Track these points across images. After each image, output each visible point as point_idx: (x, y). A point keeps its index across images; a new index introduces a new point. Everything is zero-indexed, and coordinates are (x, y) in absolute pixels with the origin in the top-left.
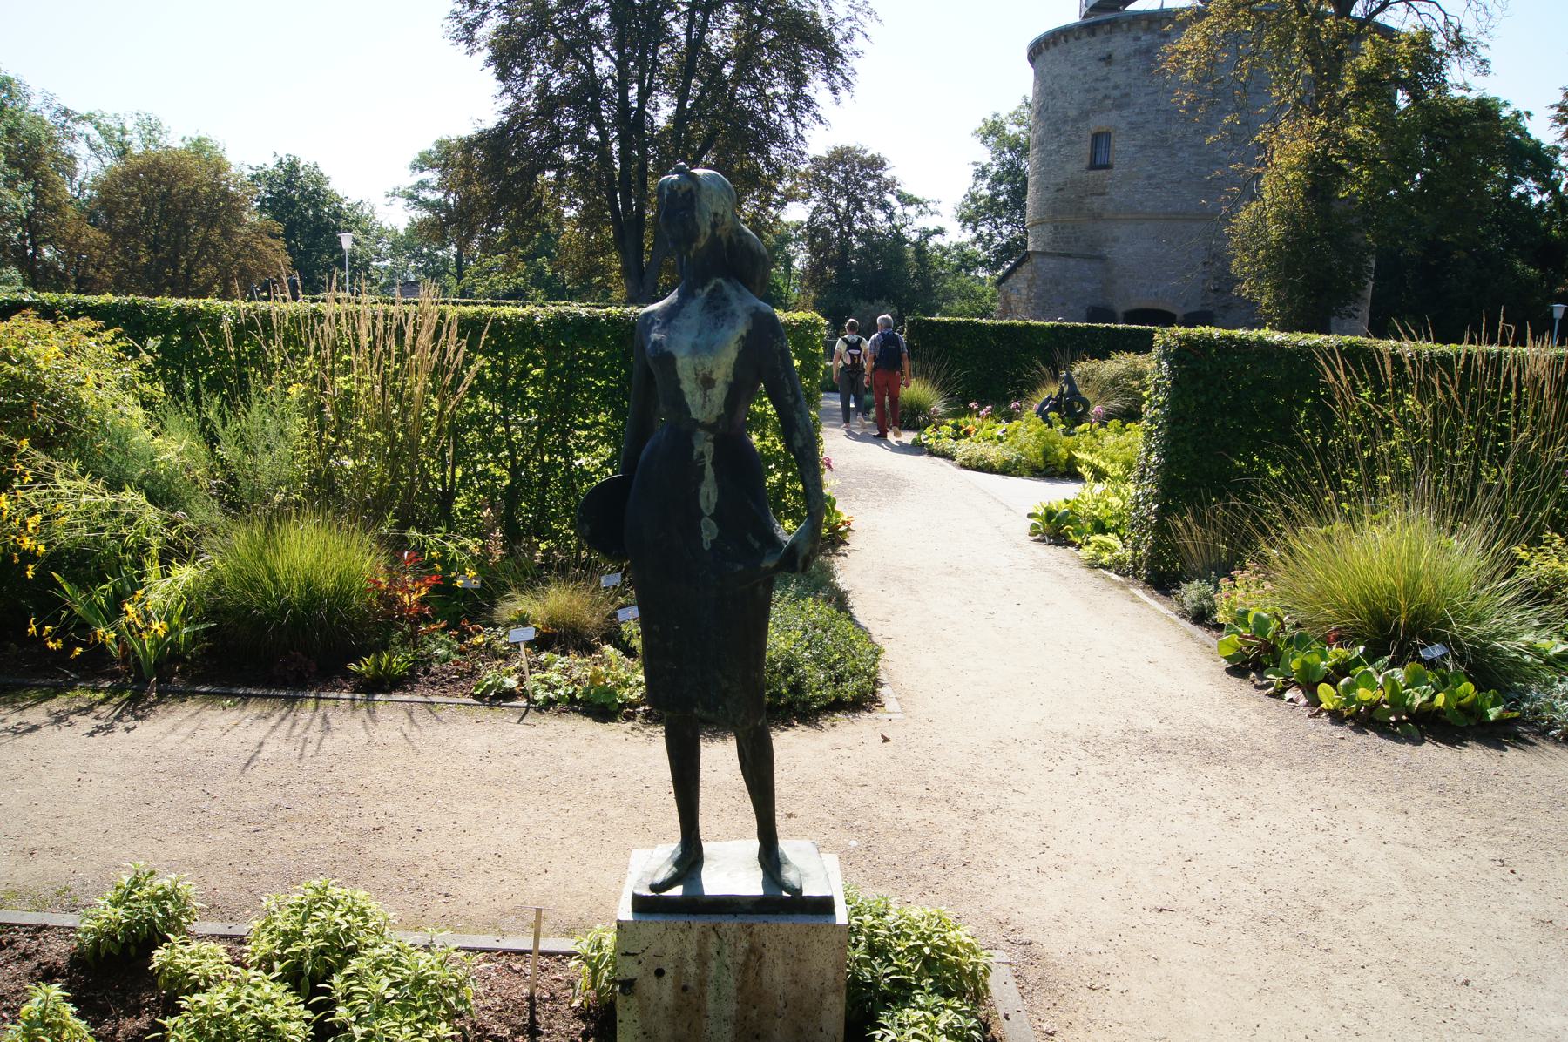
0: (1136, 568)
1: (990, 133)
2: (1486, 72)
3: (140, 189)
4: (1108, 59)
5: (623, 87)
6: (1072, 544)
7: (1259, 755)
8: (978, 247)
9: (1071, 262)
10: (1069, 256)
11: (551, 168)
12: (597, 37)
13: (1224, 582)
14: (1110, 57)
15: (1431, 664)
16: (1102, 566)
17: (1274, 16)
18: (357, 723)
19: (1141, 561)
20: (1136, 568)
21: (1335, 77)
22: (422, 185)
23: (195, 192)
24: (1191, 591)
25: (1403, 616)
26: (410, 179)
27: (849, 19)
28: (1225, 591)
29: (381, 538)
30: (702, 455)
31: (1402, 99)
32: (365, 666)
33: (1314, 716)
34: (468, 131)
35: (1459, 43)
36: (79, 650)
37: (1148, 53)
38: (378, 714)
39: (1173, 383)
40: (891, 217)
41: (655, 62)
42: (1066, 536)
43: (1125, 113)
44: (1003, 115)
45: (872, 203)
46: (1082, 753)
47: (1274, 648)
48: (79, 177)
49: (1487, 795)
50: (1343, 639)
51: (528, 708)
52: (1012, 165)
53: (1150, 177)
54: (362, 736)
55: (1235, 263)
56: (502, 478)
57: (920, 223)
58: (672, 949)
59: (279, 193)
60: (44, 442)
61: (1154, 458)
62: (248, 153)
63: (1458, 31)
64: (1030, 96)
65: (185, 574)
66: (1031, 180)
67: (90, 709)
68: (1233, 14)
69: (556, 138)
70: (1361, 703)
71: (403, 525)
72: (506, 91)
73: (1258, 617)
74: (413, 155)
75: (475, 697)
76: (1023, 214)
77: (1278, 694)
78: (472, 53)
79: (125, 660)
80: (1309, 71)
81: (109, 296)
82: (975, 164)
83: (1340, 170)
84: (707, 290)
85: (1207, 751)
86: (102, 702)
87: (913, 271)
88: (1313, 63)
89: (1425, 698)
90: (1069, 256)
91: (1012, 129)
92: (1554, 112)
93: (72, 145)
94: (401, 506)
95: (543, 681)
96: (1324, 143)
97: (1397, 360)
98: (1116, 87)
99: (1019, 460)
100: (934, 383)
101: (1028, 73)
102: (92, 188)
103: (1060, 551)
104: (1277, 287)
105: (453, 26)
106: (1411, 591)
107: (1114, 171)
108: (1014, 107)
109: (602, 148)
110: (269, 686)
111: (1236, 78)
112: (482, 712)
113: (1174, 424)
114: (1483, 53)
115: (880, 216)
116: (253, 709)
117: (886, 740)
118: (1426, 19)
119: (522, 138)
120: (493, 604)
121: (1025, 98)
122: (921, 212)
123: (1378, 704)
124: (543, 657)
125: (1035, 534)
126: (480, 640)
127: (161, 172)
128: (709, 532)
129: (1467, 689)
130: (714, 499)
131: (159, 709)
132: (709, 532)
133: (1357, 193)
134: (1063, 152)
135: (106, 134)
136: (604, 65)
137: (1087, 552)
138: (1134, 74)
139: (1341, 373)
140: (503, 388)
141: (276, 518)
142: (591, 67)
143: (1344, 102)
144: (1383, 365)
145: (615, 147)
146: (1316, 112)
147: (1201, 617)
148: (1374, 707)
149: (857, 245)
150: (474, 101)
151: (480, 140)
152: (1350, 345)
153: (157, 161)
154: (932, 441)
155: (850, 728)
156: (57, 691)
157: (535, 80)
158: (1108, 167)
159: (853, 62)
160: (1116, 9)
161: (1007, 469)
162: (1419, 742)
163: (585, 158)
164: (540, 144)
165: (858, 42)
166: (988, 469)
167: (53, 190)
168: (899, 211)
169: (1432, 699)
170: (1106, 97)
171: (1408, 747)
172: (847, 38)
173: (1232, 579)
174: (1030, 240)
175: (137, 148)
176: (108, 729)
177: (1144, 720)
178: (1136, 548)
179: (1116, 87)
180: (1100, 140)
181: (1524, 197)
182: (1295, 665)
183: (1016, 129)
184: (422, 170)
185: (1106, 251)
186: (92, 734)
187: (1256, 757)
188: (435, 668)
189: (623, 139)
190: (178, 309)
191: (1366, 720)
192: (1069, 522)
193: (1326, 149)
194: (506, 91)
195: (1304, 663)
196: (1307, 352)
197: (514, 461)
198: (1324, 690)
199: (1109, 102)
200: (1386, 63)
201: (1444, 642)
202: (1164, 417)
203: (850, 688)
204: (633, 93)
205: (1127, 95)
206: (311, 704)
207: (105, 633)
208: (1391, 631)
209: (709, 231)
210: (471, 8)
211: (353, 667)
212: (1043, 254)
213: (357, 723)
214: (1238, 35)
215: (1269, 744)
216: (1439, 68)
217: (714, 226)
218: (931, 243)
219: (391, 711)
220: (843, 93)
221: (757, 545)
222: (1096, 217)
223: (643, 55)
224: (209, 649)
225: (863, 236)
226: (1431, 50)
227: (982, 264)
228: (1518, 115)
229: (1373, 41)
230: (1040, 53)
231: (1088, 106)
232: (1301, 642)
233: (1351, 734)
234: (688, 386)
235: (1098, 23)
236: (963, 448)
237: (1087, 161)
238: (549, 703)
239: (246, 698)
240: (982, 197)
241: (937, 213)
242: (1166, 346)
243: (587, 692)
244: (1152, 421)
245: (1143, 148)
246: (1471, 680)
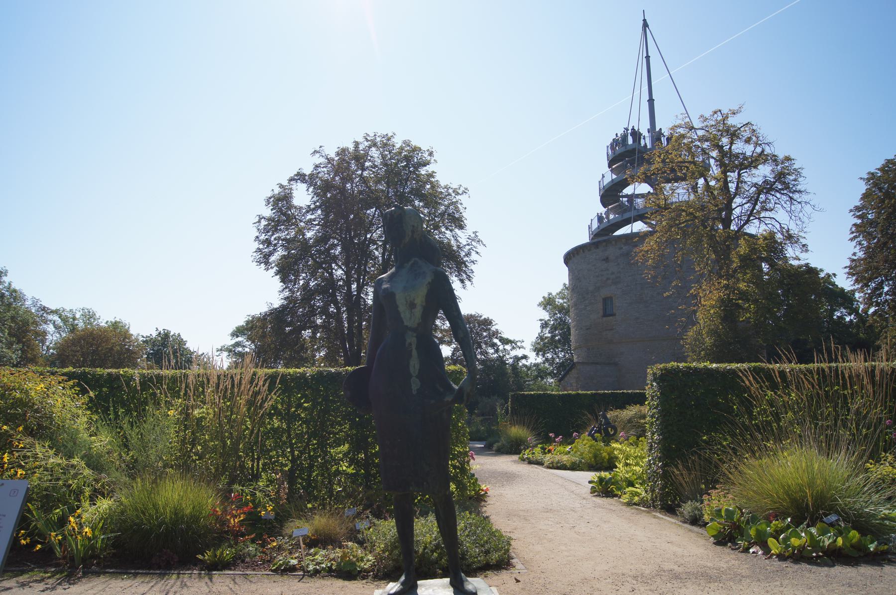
0: (654, 502)
1: (548, 304)
2: (807, 251)
3: (82, 348)
4: (606, 260)
5: (348, 283)
6: (616, 496)
7: (739, 577)
8: (547, 365)
10: (597, 363)
11: (309, 328)
12: (334, 259)
13: (705, 497)
15: (832, 525)
16: (635, 504)
17: (690, 230)
18: (203, 584)
19: (656, 497)
20: (654, 502)
21: (727, 257)
22: (238, 344)
23: (111, 349)
24: (687, 508)
25: (810, 499)
26: (230, 342)
27: (468, 245)
28: (706, 502)
29: (219, 490)
30: (410, 344)
31: (765, 267)
32: (207, 556)
33: (769, 558)
34: (263, 309)
35: (789, 237)
36: (39, 546)
37: (627, 254)
38: (214, 580)
39: (661, 394)
40: (497, 351)
41: (365, 270)
42: (612, 491)
44: (554, 294)
45: (486, 343)
46: (635, 582)
47: (739, 527)
48: (47, 344)
49: (876, 586)
50: (779, 514)
51: (304, 576)
52: (561, 320)
54: (205, 589)
56: (286, 465)
57: (513, 353)
59: (158, 351)
60: (30, 432)
61: (656, 437)
62: (142, 327)
64: (567, 283)
65: (104, 504)
66: (572, 325)
67: (42, 580)
68: (669, 230)
69: (313, 312)
70: (794, 548)
71: (232, 482)
72: (286, 288)
73: (727, 510)
74: (232, 328)
75: (272, 571)
76: (570, 346)
77: (746, 550)
78: (267, 269)
79: (64, 558)
80: (714, 256)
81: (71, 368)
82: (541, 320)
83: (738, 305)
84: (410, 263)
85: (706, 577)
86: (49, 578)
87: (511, 380)
88: (715, 252)
89: (831, 541)
90: (597, 363)
91: (559, 301)
92: (847, 270)
93: (45, 326)
94: (231, 472)
95: (313, 561)
96: (727, 292)
97: (782, 373)
98: (613, 273)
99: (580, 462)
100: (528, 427)
101: (566, 269)
102: (54, 349)
103: (609, 500)
105: (258, 256)
106: (811, 484)
108: (559, 290)
109: (338, 316)
110: (149, 569)
111: (675, 262)
112: (278, 577)
114: (803, 241)
115: (491, 351)
116: (139, 580)
117: (518, 581)
118: (770, 226)
119: (293, 312)
120: (282, 526)
121: (565, 285)
122: (514, 348)
123: (804, 547)
124: (312, 550)
125: (594, 492)
126: (275, 544)
127: (93, 339)
128: (415, 385)
129: (854, 535)
130: (417, 366)
131: (84, 580)
132: (415, 385)
133: (750, 318)
134: (588, 309)
135: (65, 320)
136: (339, 273)
137: (625, 499)
139: (751, 379)
140: (288, 414)
141: (159, 476)
142: (331, 274)
143: (735, 271)
145: (345, 316)
146: (721, 277)
147: (696, 521)
148: (802, 548)
149: (480, 367)
150: (266, 292)
151: (271, 314)
152: (755, 368)
153: (92, 333)
154: (530, 456)
155: (495, 578)
156: (22, 573)
157: (301, 282)
158: (613, 315)
159: (472, 267)
160: (608, 235)
161: (574, 467)
162: (833, 566)
163: (329, 322)
164: (303, 315)
165: (474, 256)
166: (563, 467)
167: (33, 350)
168: (501, 347)
169: (835, 541)
170: (608, 279)
171: (826, 569)
172: (468, 254)
173: (709, 494)
174: (575, 357)
175: (81, 325)
176: (53, 589)
177: (667, 566)
178: (653, 491)
180: (607, 301)
181: (841, 318)
182: (752, 532)
183: (561, 301)
184: (237, 336)
186: (43, 591)
187: (738, 578)
188: (248, 559)
189: (349, 311)
190: (109, 374)
191: (799, 557)
192: (613, 484)
193: (729, 295)
194: (286, 288)
195: (757, 530)
196: (733, 372)
197: (293, 455)
198: (771, 542)
200: (753, 250)
201: (837, 512)
202: (658, 413)
203: (495, 557)
204: (354, 286)
206: (174, 576)
207: (55, 537)
208: (806, 508)
209: (410, 234)
210: (268, 246)
211: (200, 557)
212: (583, 363)
213: (203, 584)
214: (674, 240)
215: (745, 572)
216: (781, 251)
217: (413, 232)
218: (520, 364)
219: (222, 582)
220: (467, 282)
221: (442, 390)
223: (359, 267)
224: (114, 554)
225: (482, 362)
226: (776, 242)
227: (549, 374)
228: (829, 275)
229: (744, 239)
230: (570, 259)
232: (753, 520)
233: (792, 565)
234: (402, 308)
235: (599, 242)
236: (548, 458)
237: (601, 313)
238: (316, 573)
239: (135, 575)
240: (546, 338)
241: (523, 347)
242: (654, 374)
243: (339, 565)
244: (652, 417)
246: (854, 529)
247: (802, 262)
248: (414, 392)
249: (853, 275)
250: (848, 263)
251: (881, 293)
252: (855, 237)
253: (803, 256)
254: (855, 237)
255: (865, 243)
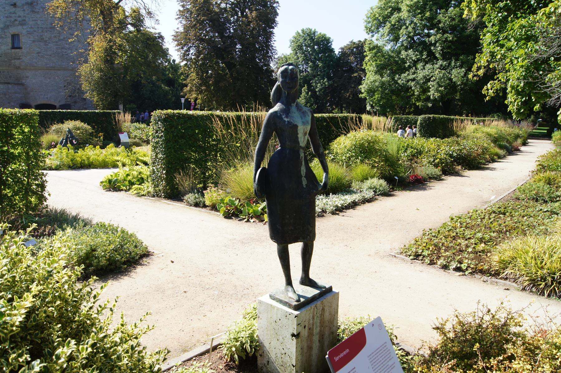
9: (10, 86)
14: (15, 4)
35: (149, 13)
42: (119, 187)
43: (25, 27)
53: (38, 53)
55: (83, 86)
58: (308, 317)
63: (148, 9)
90: (9, 83)
98: (20, 17)
103: (116, 194)
104: (98, 95)
107: (23, 50)
113: (167, 143)
114: (157, 18)
117: (173, 262)
130: (305, 171)
138: (27, 12)
144: (230, 121)
179: (20, 17)
180: (15, 37)
185: (24, 81)
199: (17, 23)
205: (25, 20)
222: (18, 68)
231: (8, 23)
237: (10, 45)
245: (34, 41)
247: (157, 31)
248: (305, 187)
249: (176, 40)
250: (174, 34)
251: (189, 54)
252: (179, 18)
253: (156, 26)
254: (179, 18)
255: (184, 22)
